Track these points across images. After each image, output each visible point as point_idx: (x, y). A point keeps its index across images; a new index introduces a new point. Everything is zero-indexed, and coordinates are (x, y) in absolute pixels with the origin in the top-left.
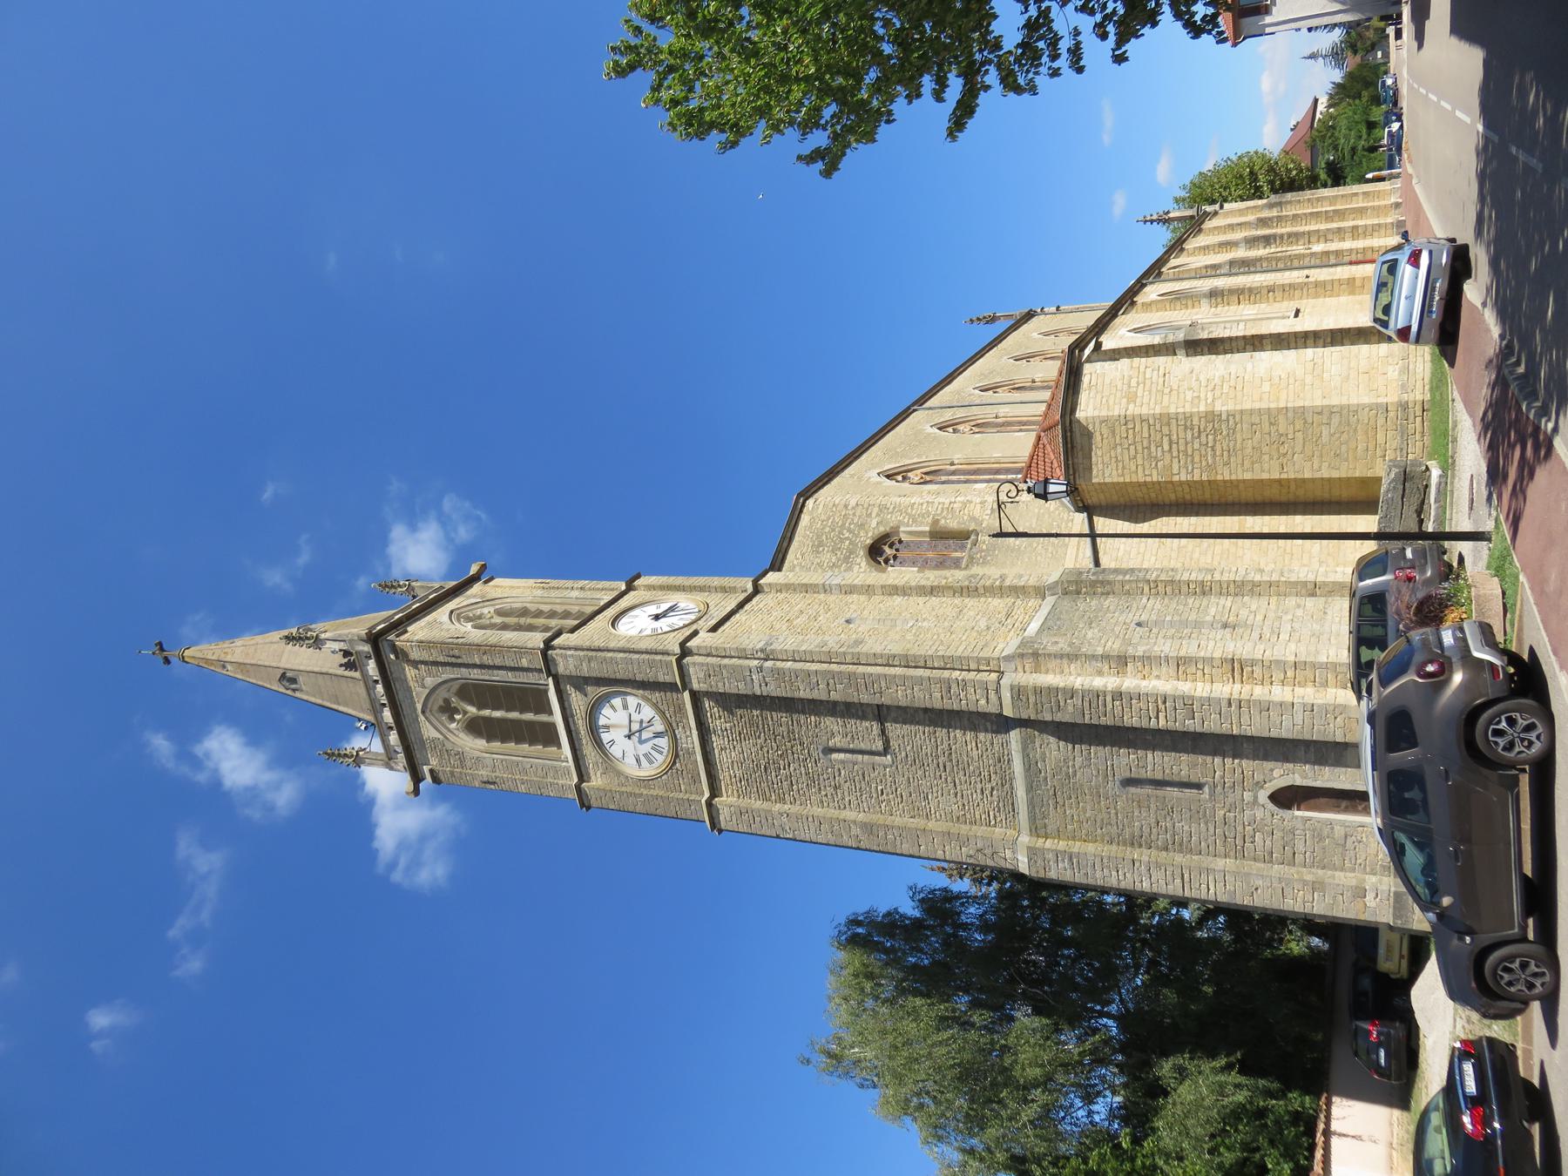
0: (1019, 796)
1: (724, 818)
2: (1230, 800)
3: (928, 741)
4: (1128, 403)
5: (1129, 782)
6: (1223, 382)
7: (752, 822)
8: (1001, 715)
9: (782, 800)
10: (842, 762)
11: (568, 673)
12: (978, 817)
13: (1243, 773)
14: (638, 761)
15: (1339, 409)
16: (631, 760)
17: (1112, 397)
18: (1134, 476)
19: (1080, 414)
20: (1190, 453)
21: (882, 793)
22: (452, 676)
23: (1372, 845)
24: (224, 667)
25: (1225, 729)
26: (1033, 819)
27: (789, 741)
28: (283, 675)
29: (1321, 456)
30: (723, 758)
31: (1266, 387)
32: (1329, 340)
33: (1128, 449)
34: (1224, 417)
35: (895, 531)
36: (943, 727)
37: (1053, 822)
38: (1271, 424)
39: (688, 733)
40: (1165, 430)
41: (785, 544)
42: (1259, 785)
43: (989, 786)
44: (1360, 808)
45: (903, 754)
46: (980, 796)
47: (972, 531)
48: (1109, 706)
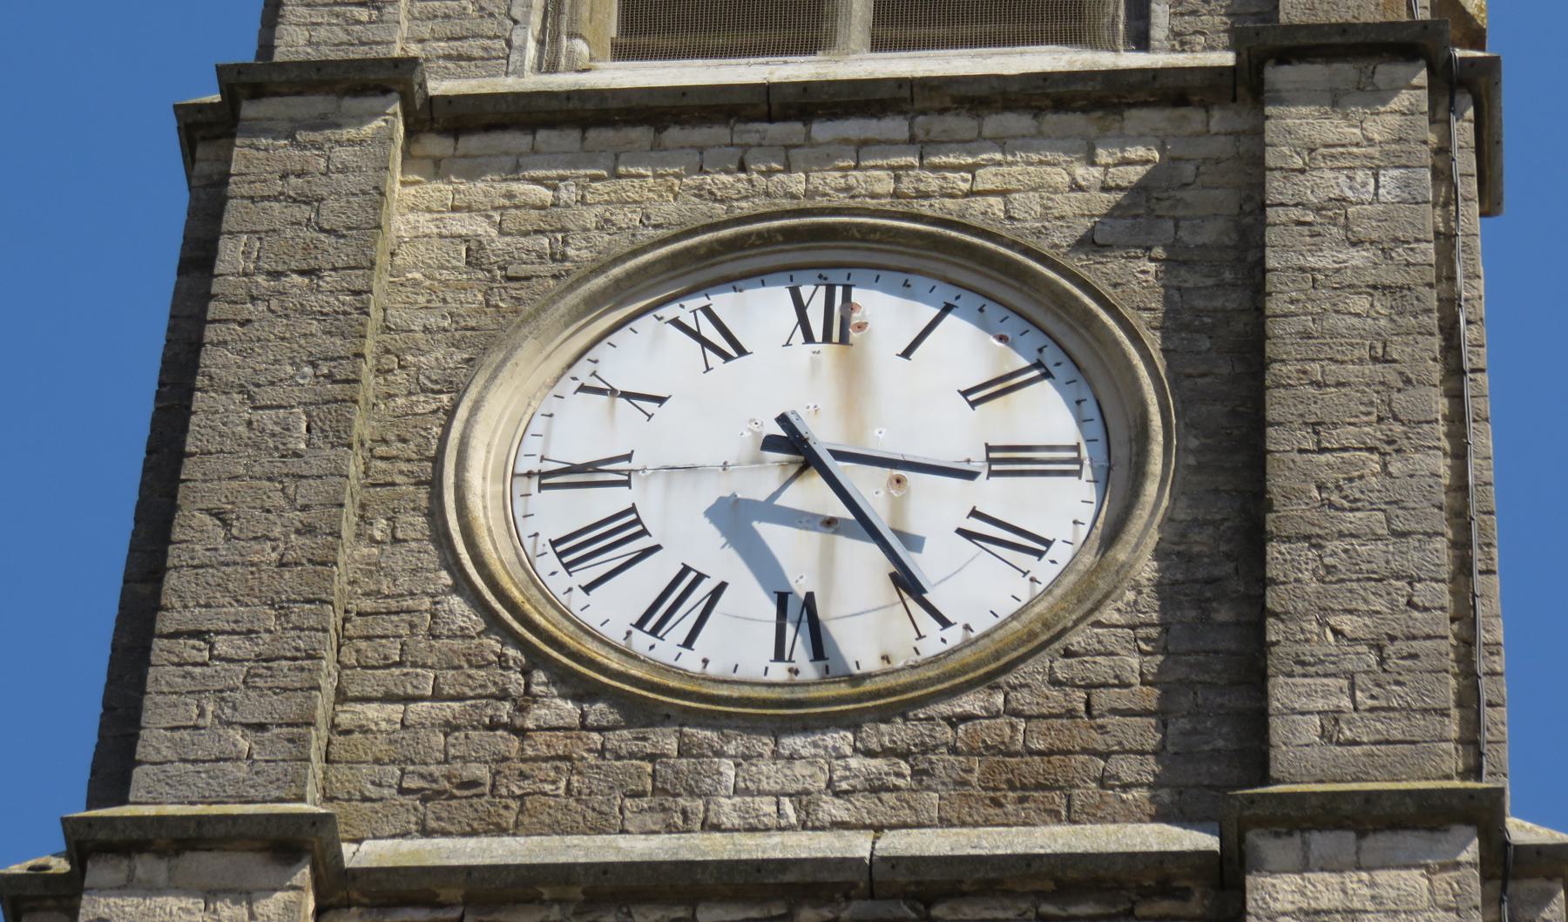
14: (582, 475)
39: (834, 809)
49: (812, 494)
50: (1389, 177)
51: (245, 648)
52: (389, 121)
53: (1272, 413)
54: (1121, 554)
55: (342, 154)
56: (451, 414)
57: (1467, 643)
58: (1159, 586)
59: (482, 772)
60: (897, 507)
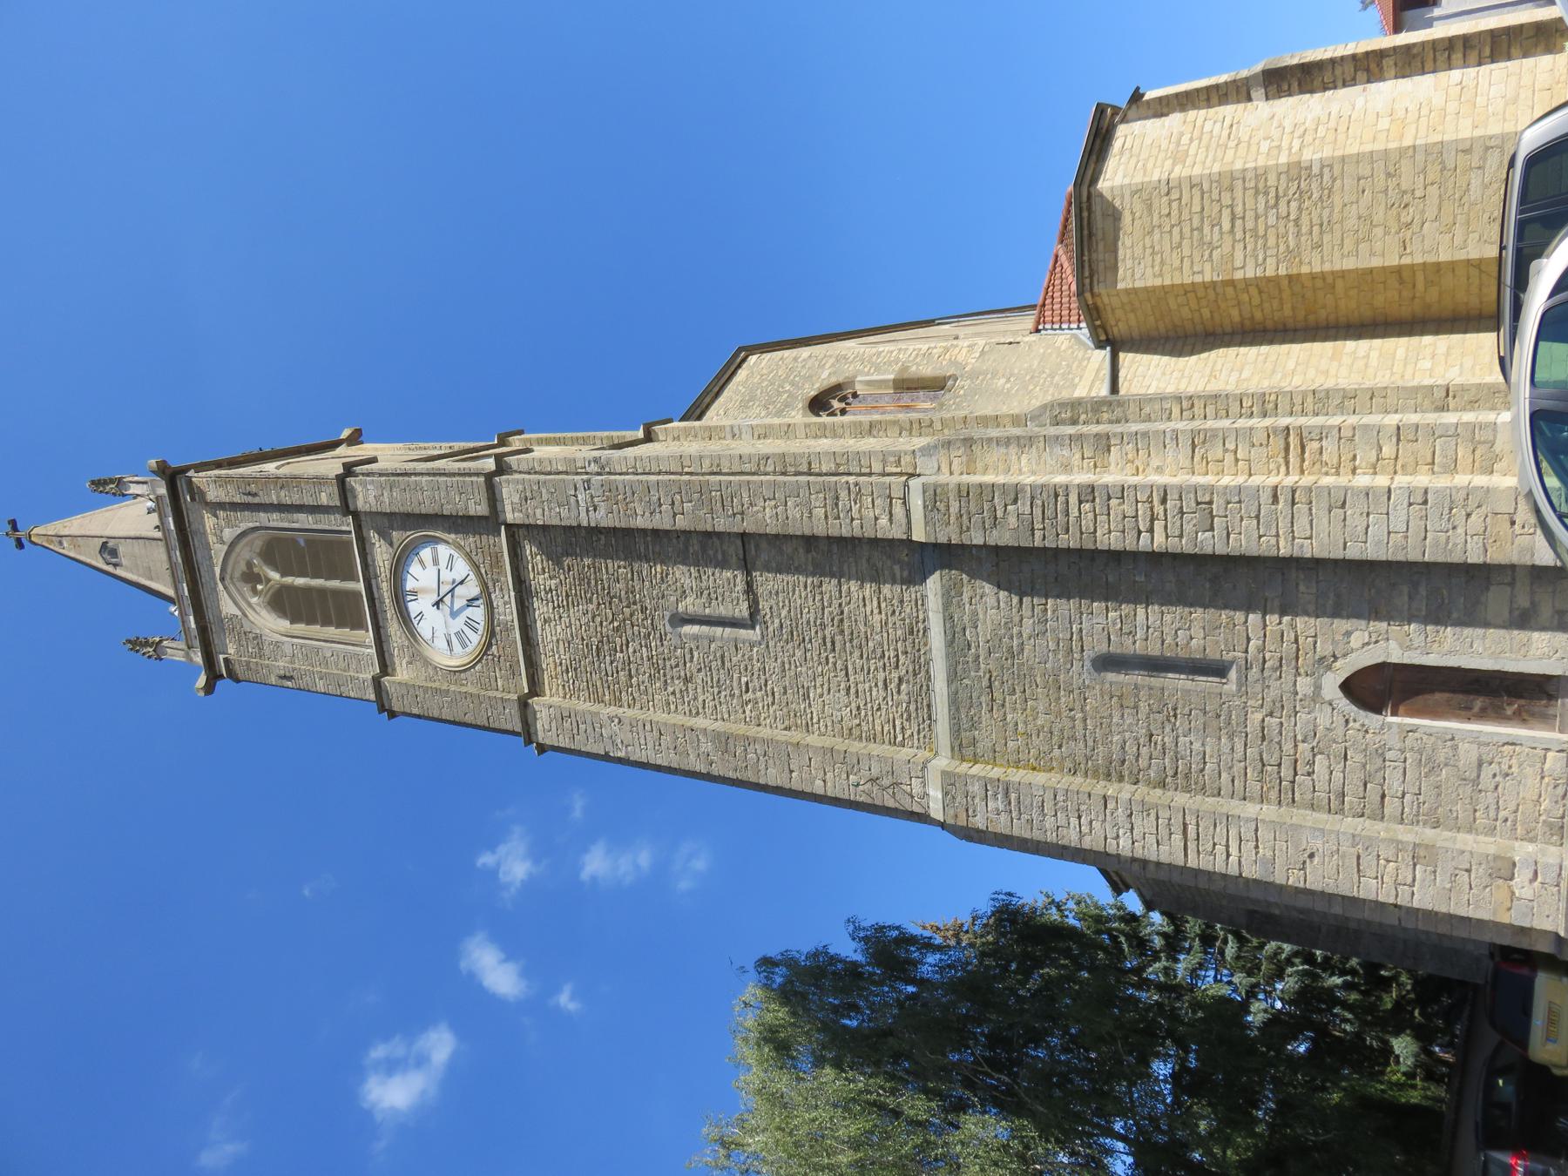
1: (545, 730)
2: (1272, 694)
3: (810, 600)
4: (1174, 165)
5: (1109, 662)
6: (1318, 125)
7: (575, 731)
8: (910, 541)
9: (617, 701)
10: (696, 637)
11: (367, 508)
12: (878, 728)
14: (449, 643)
15: (1498, 142)
16: (441, 643)
17: (1152, 160)
18: (1177, 273)
19: (1103, 185)
20: (1261, 233)
21: (747, 691)
22: (251, 525)
23: (1529, 782)
24: (61, 543)
25: (1265, 547)
26: (956, 730)
27: (628, 607)
28: (104, 545)
30: (548, 635)
31: (1384, 123)
32: (1487, 51)
33: (1170, 232)
34: (1315, 170)
35: (851, 383)
36: (832, 575)
37: (987, 735)
38: (1389, 175)
39: (506, 598)
40: (1226, 200)
41: (708, 400)
43: (895, 675)
44: (1509, 712)
45: (777, 621)
46: (882, 693)
47: (950, 376)
48: (1074, 512)
49: (447, 599)
50: (369, 487)
55: (393, 690)
58: (456, 534)
60: (448, 583)
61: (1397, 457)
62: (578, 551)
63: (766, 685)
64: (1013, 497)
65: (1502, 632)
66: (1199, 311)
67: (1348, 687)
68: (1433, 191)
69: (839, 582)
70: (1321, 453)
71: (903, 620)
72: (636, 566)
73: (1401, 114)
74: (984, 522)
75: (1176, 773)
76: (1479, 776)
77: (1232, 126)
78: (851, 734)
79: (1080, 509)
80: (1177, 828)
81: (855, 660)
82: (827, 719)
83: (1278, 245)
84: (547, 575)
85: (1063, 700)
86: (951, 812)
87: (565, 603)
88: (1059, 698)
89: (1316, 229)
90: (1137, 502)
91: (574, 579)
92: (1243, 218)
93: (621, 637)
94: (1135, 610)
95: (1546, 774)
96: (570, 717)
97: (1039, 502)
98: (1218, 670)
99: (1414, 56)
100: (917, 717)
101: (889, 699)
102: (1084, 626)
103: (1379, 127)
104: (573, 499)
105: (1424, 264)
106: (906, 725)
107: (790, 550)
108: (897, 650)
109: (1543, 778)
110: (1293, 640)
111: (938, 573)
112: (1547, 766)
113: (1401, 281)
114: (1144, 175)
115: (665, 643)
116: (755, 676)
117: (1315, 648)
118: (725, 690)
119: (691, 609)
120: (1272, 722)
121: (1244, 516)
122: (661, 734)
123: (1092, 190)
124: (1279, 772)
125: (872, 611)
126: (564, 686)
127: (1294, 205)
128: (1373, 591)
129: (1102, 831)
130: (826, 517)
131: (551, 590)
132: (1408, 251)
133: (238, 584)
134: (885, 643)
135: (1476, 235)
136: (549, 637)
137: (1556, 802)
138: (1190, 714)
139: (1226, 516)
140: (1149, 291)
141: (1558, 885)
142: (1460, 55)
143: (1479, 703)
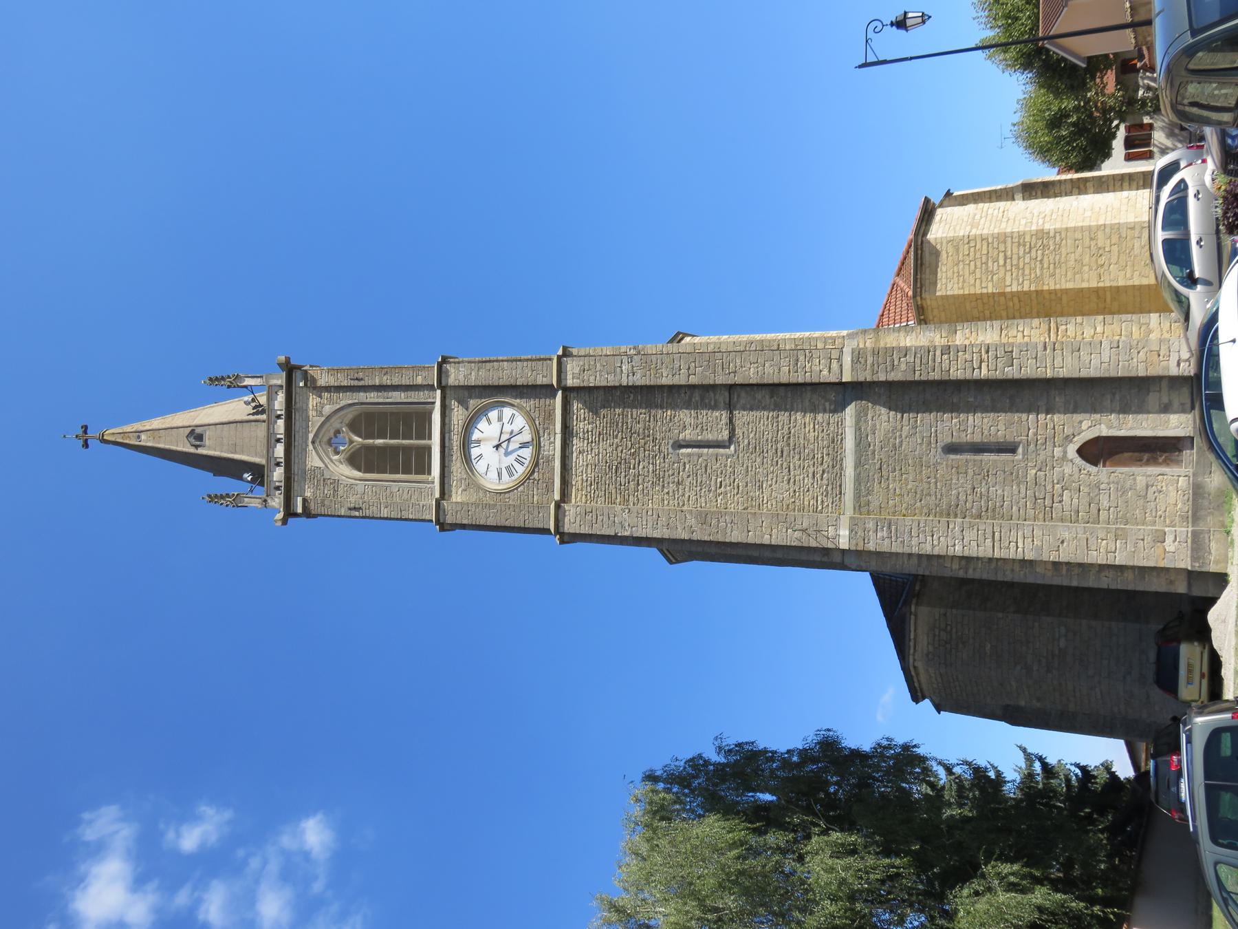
0: (847, 474)
2: (1041, 458)
3: (770, 426)
4: (971, 228)
5: (952, 449)
10: (689, 455)
12: (806, 503)
13: (1054, 428)
14: (500, 475)
16: (493, 475)
18: (972, 288)
20: (1021, 266)
22: (350, 402)
26: (857, 496)
28: (192, 432)
29: (1133, 265)
30: (579, 461)
32: (1141, 183)
33: (969, 264)
34: (1052, 234)
36: (786, 410)
38: (1091, 239)
39: (552, 439)
40: (1002, 248)
42: (1069, 439)
43: (820, 469)
45: (746, 442)
46: (811, 481)
49: (504, 445)
51: (527, 515)
52: (445, 503)
53: (497, 384)
54: (516, 404)
56: (490, 492)
57: (531, 360)
59: (545, 485)
60: (507, 433)
61: (1104, 333)
62: (613, 405)
63: (734, 482)
64: (904, 353)
65: (1156, 415)
66: (983, 312)
67: (1080, 452)
68: (1115, 248)
69: (790, 414)
70: (1067, 331)
71: (829, 435)
72: (653, 412)
73: (1097, 209)
74: (886, 368)
75: (988, 509)
76: (1147, 493)
77: (1004, 212)
78: (788, 508)
79: (941, 358)
80: (989, 535)
81: (796, 461)
82: (773, 501)
83: (1030, 274)
84: (586, 422)
85: (924, 472)
86: (854, 542)
87: (597, 439)
88: (922, 472)
89: (1052, 266)
90: (973, 353)
91: (607, 423)
92: (1011, 258)
93: (635, 460)
94: (968, 417)
95: (1179, 489)
96: (592, 512)
97: (919, 356)
98: (1011, 449)
99: (1104, 182)
100: (832, 494)
101: (815, 484)
102: (938, 428)
103: (1086, 215)
104: (618, 369)
105: (1111, 286)
106: (825, 499)
107: (760, 397)
108: (823, 453)
109: (1178, 491)
110: (1052, 427)
111: (854, 403)
112: (1179, 485)
113: (1098, 297)
114: (955, 232)
115: (667, 460)
116: (727, 477)
117: (1064, 431)
118: (705, 488)
119: (688, 437)
120: (1041, 474)
121: (1030, 357)
122: (659, 517)
123: (924, 239)
124: (1044, 503)
125: (809, 431)
126: (586, 495)
127: (1039, 252)
128: (1093, 399)
129: (946, 542)
130: (789, 372)
131: (588, 432)
132: (1102, 280)
133: (324, 446)
134: (816, 449)
135: (1137, 273)
136: (581, 462)
137: (1185, 504)
138: (996, 474)
139: (1020, 358)
140: (955, 297)
141: (1187, 542)
142: (1127, 184)
143: (1146, 456)
